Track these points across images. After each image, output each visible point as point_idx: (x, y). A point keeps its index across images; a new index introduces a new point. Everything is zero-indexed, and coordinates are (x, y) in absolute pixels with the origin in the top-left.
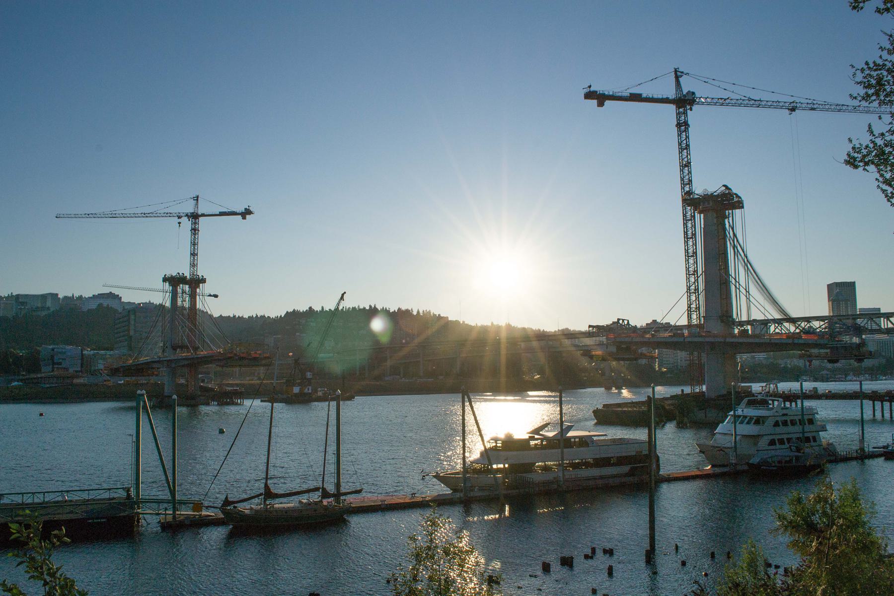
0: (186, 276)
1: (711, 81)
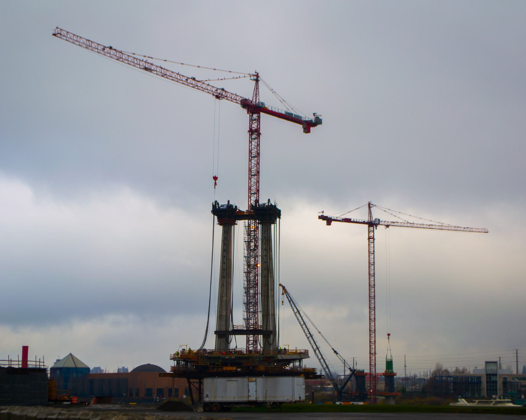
0: (459, 402)
1: (388, 211)
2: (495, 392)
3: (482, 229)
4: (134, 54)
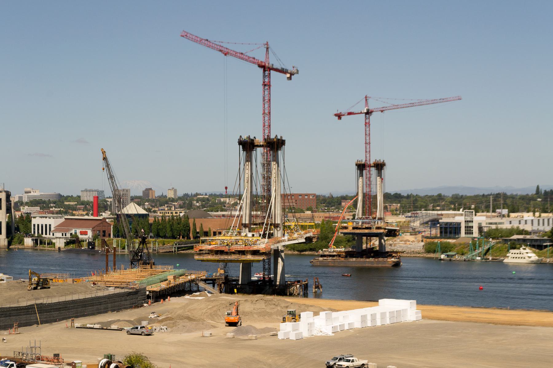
3: (453, 97)
4: (215, 41)
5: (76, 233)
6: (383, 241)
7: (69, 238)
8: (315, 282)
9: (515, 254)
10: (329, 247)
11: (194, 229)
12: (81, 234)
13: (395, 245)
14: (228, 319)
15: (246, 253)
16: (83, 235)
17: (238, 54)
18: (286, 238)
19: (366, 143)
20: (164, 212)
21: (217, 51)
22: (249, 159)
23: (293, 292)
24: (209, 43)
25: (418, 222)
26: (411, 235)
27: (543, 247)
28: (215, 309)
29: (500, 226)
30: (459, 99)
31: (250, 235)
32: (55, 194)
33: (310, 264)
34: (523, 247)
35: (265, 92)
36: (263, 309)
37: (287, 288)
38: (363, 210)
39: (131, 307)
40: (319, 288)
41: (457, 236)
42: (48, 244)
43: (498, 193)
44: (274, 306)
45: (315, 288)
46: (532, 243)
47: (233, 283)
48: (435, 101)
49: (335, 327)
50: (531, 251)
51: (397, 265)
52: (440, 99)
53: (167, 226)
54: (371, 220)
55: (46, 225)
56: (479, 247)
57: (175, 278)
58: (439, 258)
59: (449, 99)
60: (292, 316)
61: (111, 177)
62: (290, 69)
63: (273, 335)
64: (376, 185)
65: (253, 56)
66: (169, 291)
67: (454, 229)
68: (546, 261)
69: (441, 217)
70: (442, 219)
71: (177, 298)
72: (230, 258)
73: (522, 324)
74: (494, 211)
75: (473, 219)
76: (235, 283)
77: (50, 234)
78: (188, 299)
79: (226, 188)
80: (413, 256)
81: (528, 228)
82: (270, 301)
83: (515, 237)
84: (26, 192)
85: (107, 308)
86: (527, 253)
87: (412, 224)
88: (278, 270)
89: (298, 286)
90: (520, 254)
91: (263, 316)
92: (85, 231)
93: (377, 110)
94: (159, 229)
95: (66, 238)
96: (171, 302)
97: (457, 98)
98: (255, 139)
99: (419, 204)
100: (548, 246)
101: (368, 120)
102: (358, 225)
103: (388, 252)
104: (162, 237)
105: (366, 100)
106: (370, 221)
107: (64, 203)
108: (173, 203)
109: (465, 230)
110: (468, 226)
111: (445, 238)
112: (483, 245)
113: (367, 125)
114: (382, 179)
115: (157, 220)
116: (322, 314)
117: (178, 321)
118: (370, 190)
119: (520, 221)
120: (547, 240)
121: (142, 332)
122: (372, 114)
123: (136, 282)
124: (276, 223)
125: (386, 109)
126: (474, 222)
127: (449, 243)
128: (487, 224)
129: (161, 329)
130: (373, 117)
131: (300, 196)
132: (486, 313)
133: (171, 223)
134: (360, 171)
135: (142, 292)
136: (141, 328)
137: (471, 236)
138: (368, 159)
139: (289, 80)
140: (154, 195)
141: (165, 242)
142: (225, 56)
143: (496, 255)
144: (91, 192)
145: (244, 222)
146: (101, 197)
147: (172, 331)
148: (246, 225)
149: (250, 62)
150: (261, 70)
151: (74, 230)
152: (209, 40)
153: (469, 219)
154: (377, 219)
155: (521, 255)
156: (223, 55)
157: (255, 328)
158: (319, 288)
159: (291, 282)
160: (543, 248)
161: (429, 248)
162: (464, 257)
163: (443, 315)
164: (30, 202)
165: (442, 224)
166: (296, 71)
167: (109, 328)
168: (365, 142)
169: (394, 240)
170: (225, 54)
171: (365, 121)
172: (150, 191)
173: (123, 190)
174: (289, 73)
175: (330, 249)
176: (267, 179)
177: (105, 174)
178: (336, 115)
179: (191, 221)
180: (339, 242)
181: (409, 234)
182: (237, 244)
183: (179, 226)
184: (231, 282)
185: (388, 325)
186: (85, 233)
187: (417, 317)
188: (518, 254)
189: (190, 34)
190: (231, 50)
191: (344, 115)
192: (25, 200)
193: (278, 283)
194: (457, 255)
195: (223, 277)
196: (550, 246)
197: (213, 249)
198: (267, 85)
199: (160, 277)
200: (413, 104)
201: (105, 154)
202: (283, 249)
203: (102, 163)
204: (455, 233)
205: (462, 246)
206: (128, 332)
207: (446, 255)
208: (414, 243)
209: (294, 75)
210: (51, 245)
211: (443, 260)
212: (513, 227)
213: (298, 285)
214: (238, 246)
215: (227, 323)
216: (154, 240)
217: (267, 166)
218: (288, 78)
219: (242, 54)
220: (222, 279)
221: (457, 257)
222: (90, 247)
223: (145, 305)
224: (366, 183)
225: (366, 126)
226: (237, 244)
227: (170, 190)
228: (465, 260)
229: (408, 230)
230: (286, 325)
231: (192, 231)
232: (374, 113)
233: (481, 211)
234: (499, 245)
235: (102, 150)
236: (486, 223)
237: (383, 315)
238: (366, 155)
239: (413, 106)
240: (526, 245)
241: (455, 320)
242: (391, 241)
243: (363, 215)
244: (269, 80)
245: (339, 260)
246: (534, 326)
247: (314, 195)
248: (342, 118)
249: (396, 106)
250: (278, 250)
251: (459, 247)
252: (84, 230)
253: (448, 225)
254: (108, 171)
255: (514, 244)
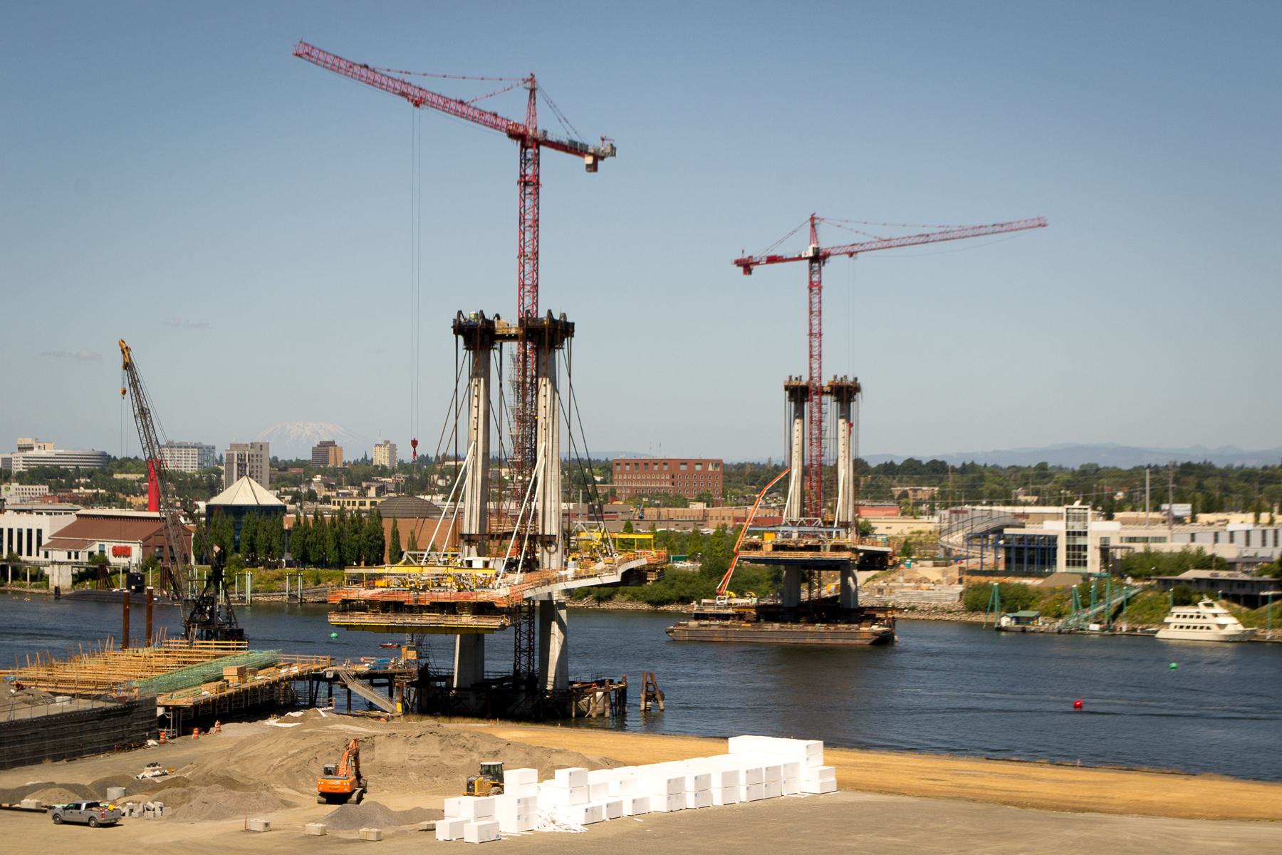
2: (1071, 559)
4: (389, 70)
5: (102, 552)
6: (850, 579)
7: (85, 565)
8: (647, 683)
9: (1185, 616)
10: (718, 594)
11: (393, 544)
12: (115, 555)
13: (891, 590)
14: (325, 784)
15: (459, 608)
16: (120, 556)
17: (452, 104)
18: (570, 572)
19: (811, 334)
20: (344, 502)
21: (396, 96)
22: (481, 370)
23: (586, 710)
24: (371, 75)
25: (961, 534)
26: (935, 565)
27: (1260, 600)
28: (305, 756)
29: (1154, 547)
30: (1040, 225)
31: (478, 562)
32: (93, 453)
33: (667, 638)
34: (1208, 601)
35: (524, 201)
36: (434, 757)
37: (571, 700)
38: (803, 505)
39: (110, 749)
40: (656, 700)
41: (1047, 570)
42: (33, 578)
43: (1185, 461)
44: (463, 750)
45: (646, 700)
46: (1231, 590)
47: (438, 684)
48: (983, 230)
49: (593, 809)
50: (1226, 611)
51: (884, 641)
52: (994, 225)
53: (328, 537)
54: (820, 527)
55: (30, 531)
56: (1100, 597)
57: (242, 672)
58: (996, 626)
59: (1015, 226)
60: (493, 780)
61: (143, 413)
62: (594, 143)
63: (426, 830)
64: (837, 439)
65: (494, 110)
66: (225, 705)
67: (1039, 550)
68: (1264, 637)
69: (1024, 521)
70: (1024, 527)
71: (244, 724)
72: (419, 622)
73: (1090, 806)
74: (1157, 509)
75: (1087, 528)
76: (443, 684)
77: (38, 555)
78: (271, 726)
79: (414, 443)
80: (933, 619)
81: (1227, 551)
82: (452, 737)
83: (1191, 574)
84: (21, 449)
85: (43, 751)
86: (1216, 615)
87: (944, 539)
88: (551, 653)
89: (599, 694)
90: (1198, 617)
91: (431, 777)
92: (126, 547)
93: (838, 251)
94: (308, 542)
95: (76, 563)
96: (221, 735)
97: (1037, 223)
98: (499, 318)
99: (988, 486)
100: (1270, 599)
101: (818, 276)
102: (786, 540)
103: (863, 609)
104: (316, 565)
105: (813, 226)
106: (816, 529)
107: (112, 475)
108: (383, 480)
109: (1068, 556)
110: (1074, 546)
111: (1017, 575)
112: (1107, 594)
113: (815, 289)
114: (851, 425)
115: (302, 522)
116: (561, 775)
117: (197, 788)
118: (820, 451)
119: (1216, 534)
120: (1270, 583)
121: (91, 818)
122: (827, 260)
123: (135, 684)
124: (547, 533)
125: (862, 248)
126: (1089, 534)
127: (1025, 586)
128: (1124, 540)
129: (148, 810)
130: (828, 268)
131: (682, 464)
132: (1012, 776)
133: (337, 529)
134: (796, 403)
135: (144, 709)
136: (88, 806)
137: (1082, 570)
138: (815, 375)
139: (590, 171)
140: (341, 458)
141: (320, 578)
142: (416, 108)
143: (1140, 618)
144: (183, 449)
145: (466, 531)
146: (207, 461)
147: (172, 816)
148: (472, 538)
149: (485, 123)
150: (515, 146)
151: (98, 543)
152: (371, 66)
153: (1078, 527)
154: (835, 525)
155: (1200, 620)
156: (411, 105)
157: (385, 810)
158: (656, 700)
159: (585, 683)
160: (1260, 603)
161: (975, 599)
162: (1059, 624)
163: (893, 780)
164: (29, 472)
165: (1010, 540)
166: (608, 150)
167: (17, 805)
168: (808, 332)
169: (889, 579)
170: (416, 102)
171: (811, 278)
172: (331, 449)
173: (253, 446)
174: (590, 154)
175: (719, 599)
176: (527, 421)
177: (127, 406)
178: (738, 263)
179: (387, 525)
180: (752, 583)
181: (931, 563)
182: (439, 585)
183: (356, 537)
184: (432, 683)
185: (742, 805)
186: (125, 552)
187: (822, 784)
188: (1191, 617)
189: (320, 50)
190: (433, 94)
191: (757, 263)
192: (18, 466)
193: (549, 687)
194: (1040, 618)
195: (415, 669)
196: (1275, 598)
197: (376, 598)
198: (530, 184)
199: (206, 670)
200: (928, 236)
201: (129, 354)
202: (563, 599)
203: (119, 377)
204: (1043, 563)
205: (1057, 595)
206: (55, 817)
207: (1012, 618)
208: (938, 587)
209: (605, 159)
210: (41, 581)
211: (1005, 629)
212: (1188, 550)
213: (600, 691)
214: (442, 590)
215: (323, 794)
216: (293, 570)
217: (526, 389)
218: (588, 166)
219: (462, 103)
220: (410, 673)
221: (1040, 624)
222: (133, 587)
223: (151, 742)
224: (811, 433)
225: (811, 291)
226: (439, 585)
227: (380, 446)
228: (1059, 632)
229: (934, 553)
230: (459, 803)
231: (390, 550)
232: (831, 258)
233: (1130, 507)
234: (1150, 594)
235: (120, 345)
236: (1122, 538)
237: (729, 779)
238: (810, 364)
239: (927, 242)
240: (1214, 597)
241: (921, 793)
242: (882, 581)
243: (802, 514)
244: (534, 170)
245: (739, 627)
246: (1121, 813)
247: (718, 463)
248: (753, 272)
249: (885, 240)
250: (552, 601)
251: (1051, 599)
252: (123, 545)
253: (1026, 541)
254: (134, 398)
255: (1185, 592)
